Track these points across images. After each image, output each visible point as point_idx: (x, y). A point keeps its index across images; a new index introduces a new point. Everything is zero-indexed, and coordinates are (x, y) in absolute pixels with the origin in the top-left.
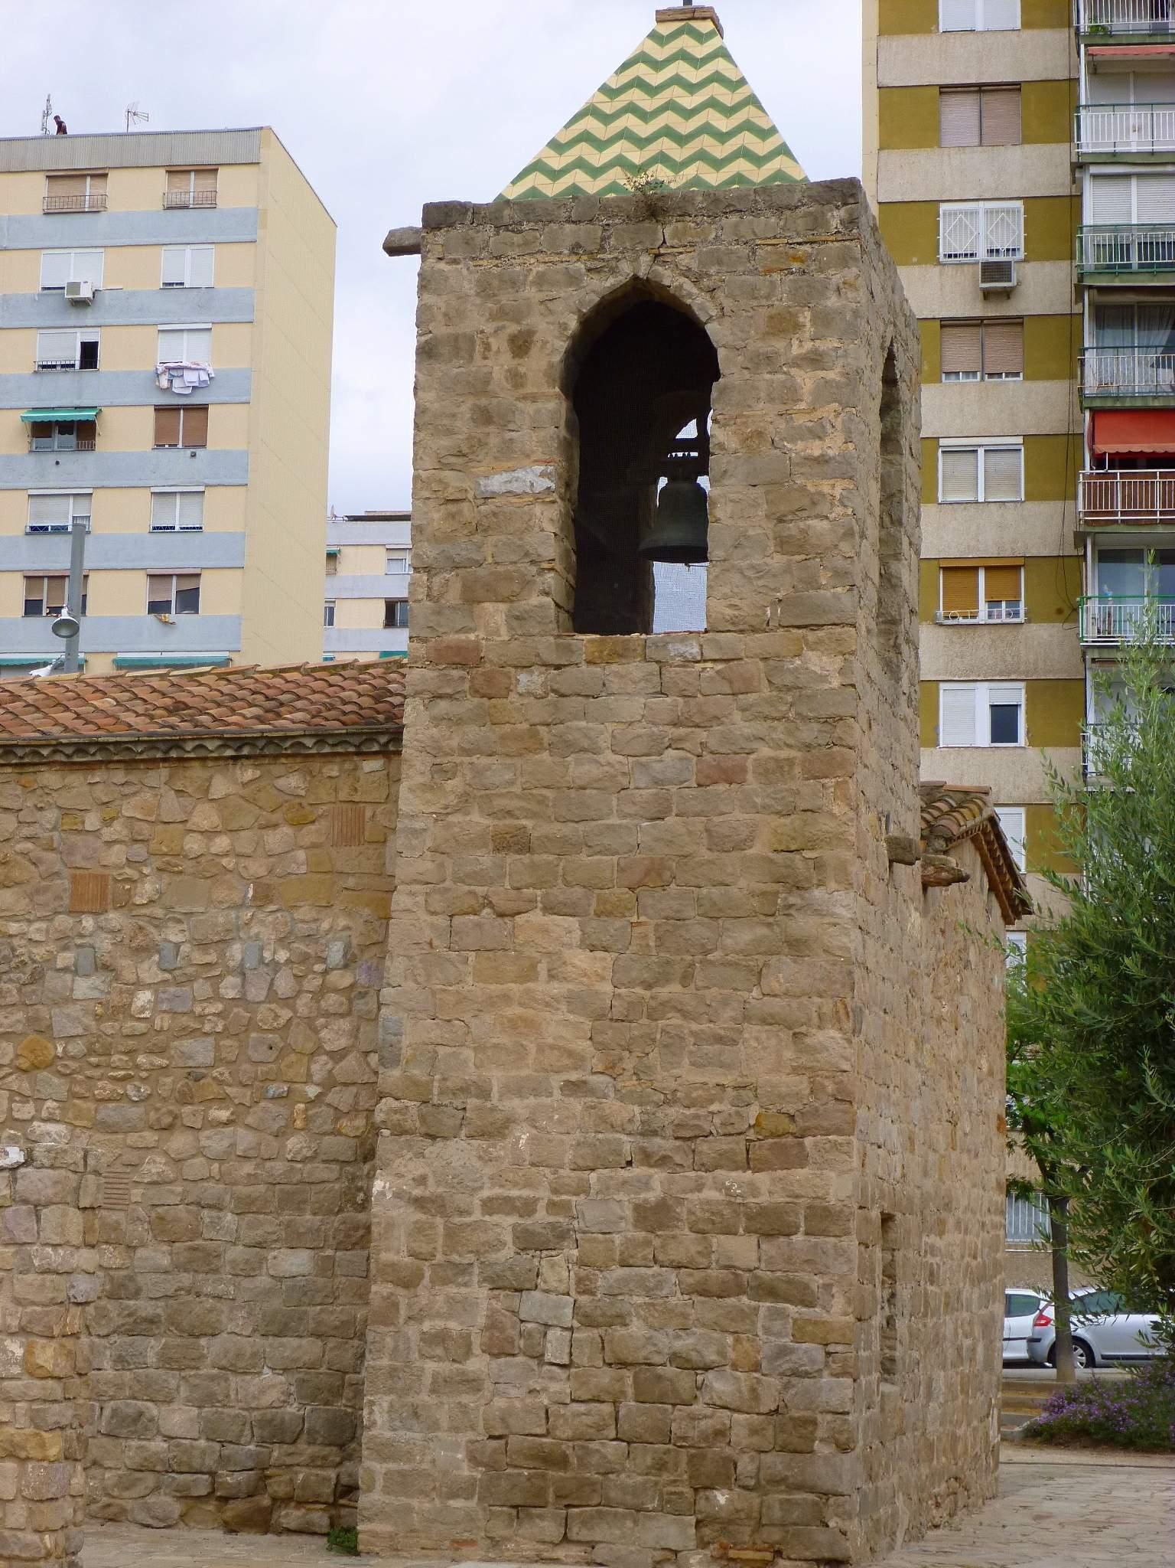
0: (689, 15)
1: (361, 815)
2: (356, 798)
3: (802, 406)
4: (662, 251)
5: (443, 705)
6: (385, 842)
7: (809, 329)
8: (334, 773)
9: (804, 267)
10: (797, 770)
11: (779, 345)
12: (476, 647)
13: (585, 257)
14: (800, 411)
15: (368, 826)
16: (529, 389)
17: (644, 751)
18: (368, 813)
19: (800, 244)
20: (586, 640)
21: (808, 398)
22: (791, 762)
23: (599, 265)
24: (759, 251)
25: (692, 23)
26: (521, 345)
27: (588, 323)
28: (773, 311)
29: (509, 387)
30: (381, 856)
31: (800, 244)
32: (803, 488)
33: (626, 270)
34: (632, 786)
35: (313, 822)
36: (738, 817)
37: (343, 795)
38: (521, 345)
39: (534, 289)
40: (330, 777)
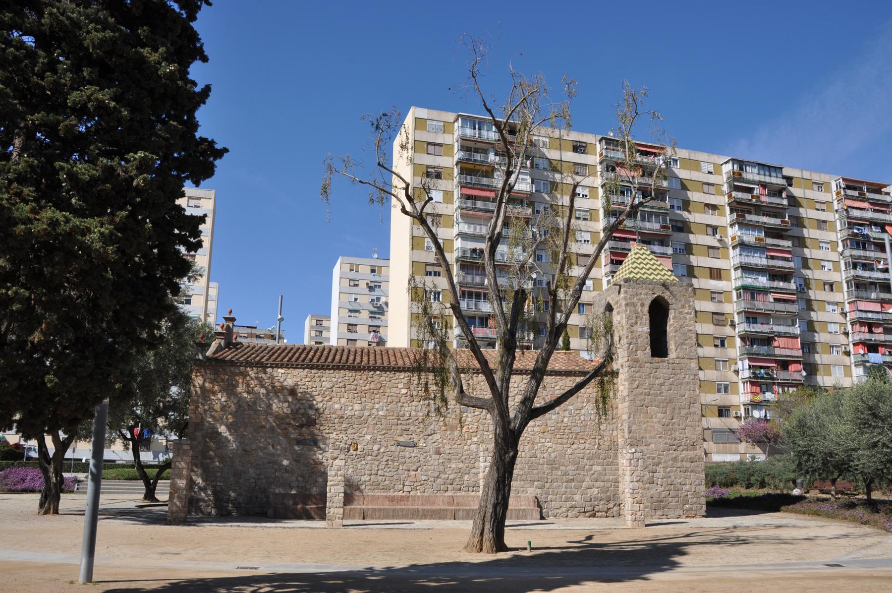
27: (652, 302)
33: (658, 294)
38: (643, 305)
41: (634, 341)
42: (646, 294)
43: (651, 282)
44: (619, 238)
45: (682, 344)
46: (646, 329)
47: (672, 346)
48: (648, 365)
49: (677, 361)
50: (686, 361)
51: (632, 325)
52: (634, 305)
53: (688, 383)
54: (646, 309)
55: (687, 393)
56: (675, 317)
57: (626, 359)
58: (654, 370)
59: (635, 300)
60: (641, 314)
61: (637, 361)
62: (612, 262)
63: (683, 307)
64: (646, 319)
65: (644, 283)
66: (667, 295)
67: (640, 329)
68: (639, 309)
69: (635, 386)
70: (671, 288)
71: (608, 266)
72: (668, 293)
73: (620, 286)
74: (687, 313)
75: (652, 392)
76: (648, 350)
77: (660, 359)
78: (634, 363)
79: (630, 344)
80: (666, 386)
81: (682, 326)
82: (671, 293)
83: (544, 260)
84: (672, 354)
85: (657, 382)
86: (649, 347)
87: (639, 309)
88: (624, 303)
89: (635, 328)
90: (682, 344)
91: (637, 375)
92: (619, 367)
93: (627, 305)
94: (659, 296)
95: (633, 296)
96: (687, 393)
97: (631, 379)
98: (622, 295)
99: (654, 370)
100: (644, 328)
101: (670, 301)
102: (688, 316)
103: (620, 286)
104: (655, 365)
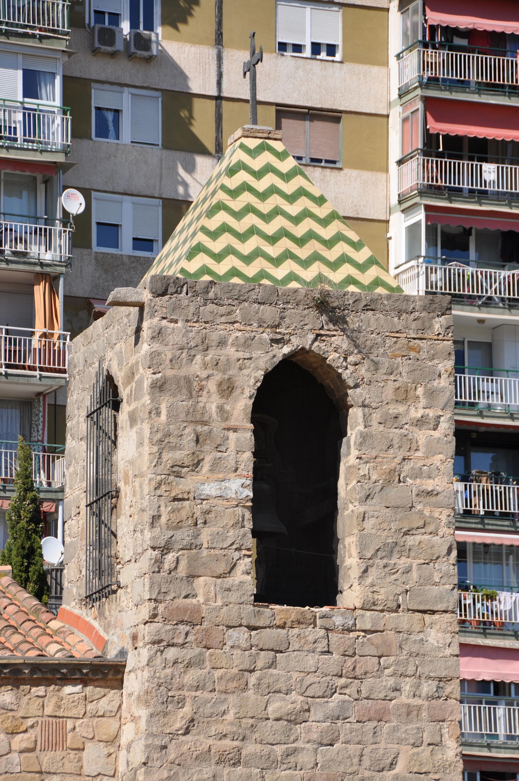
0: (265, 135)
1: (64, 727)
2: (60, 713)
3: (419, 454)
4: (322, 332)
5: (171, 653)
6: (83, 749)
7: (423, 402)
8: (41, 693)
9: (418, 356)
10: (424, 714)
11: (401, 409)
12: (197, 609)
13: (268, 330)
14: (419, 458)
15: (70, 736)
16: (232, 423)
17: (320, 694)
18: (70, 726)
19: (414, 339)
20: (280, 611)
21: (422, 449)
22: (419, 708)
23: (279, 337)
24: (387, 341)
25: (268, 141)
26: (227, 389)
27: (268, 377)
28: (397, 384)
29: (219, 419)
30: (80, 760)
31: (414, 339)
32: (421, 512)
33: (296, 343)
34: (311, 719)
35: (26, 731)
36: (385, 747)
37: (48, 711)
38: (227, 389)
39: (233, 349)
40: (38, 696)
41: (183, 536)
42: (247, 344)
43: (275, 296)
44: (471, 34)
45: (391, 549)
46: (239, 487)
47: (350, 558)
48: (241, 636)
49: (367, 620)
50: (404, 619)
51: (176, 471)
52: (191, 388)
53: (409, 711)
54: (242, 404)
55: (406, 753)
56: (364, 438)
57: (145, 612)
58: (264, 658)
59: (196, 368)
60: (217, 426)
61: (192, 620)
62: (430, 144)
63: (404, 396)
64: (240, 444)
65: (240, 299)
66: (334, 349)
67: (210, 489)
68: (211, 403)
69: (179, 724)
70: (354, 321)
71: (414, 166)
72: (340, 341)
73: (141, 307)
74: (420, 422)
75: (250, 748)
76: (244, 577)
77: (293, 612)
78: (178, 624)
79: (166, 549)
80: (315, 727)
81: (394, 477)
82: (353, 341)
83: (127, 133)
84: (351, 594)
85: (277, 706)
86: (246, 564)
87: (211, 403)
88: (147, 377)
89: (187, 484)
90: (391, 549)
91: (192, 676)
92: (128, 645)
93: (159, 387)
94: (302, 352)
95: (188, 350)
96: (406, 753)
97: (165, 697)
98: (145, 348)
99: (264, 658)
100: (229, 484)
101: (346, 375)
102: (422, 436)
103: (141, 307)
104: (269, 637)
